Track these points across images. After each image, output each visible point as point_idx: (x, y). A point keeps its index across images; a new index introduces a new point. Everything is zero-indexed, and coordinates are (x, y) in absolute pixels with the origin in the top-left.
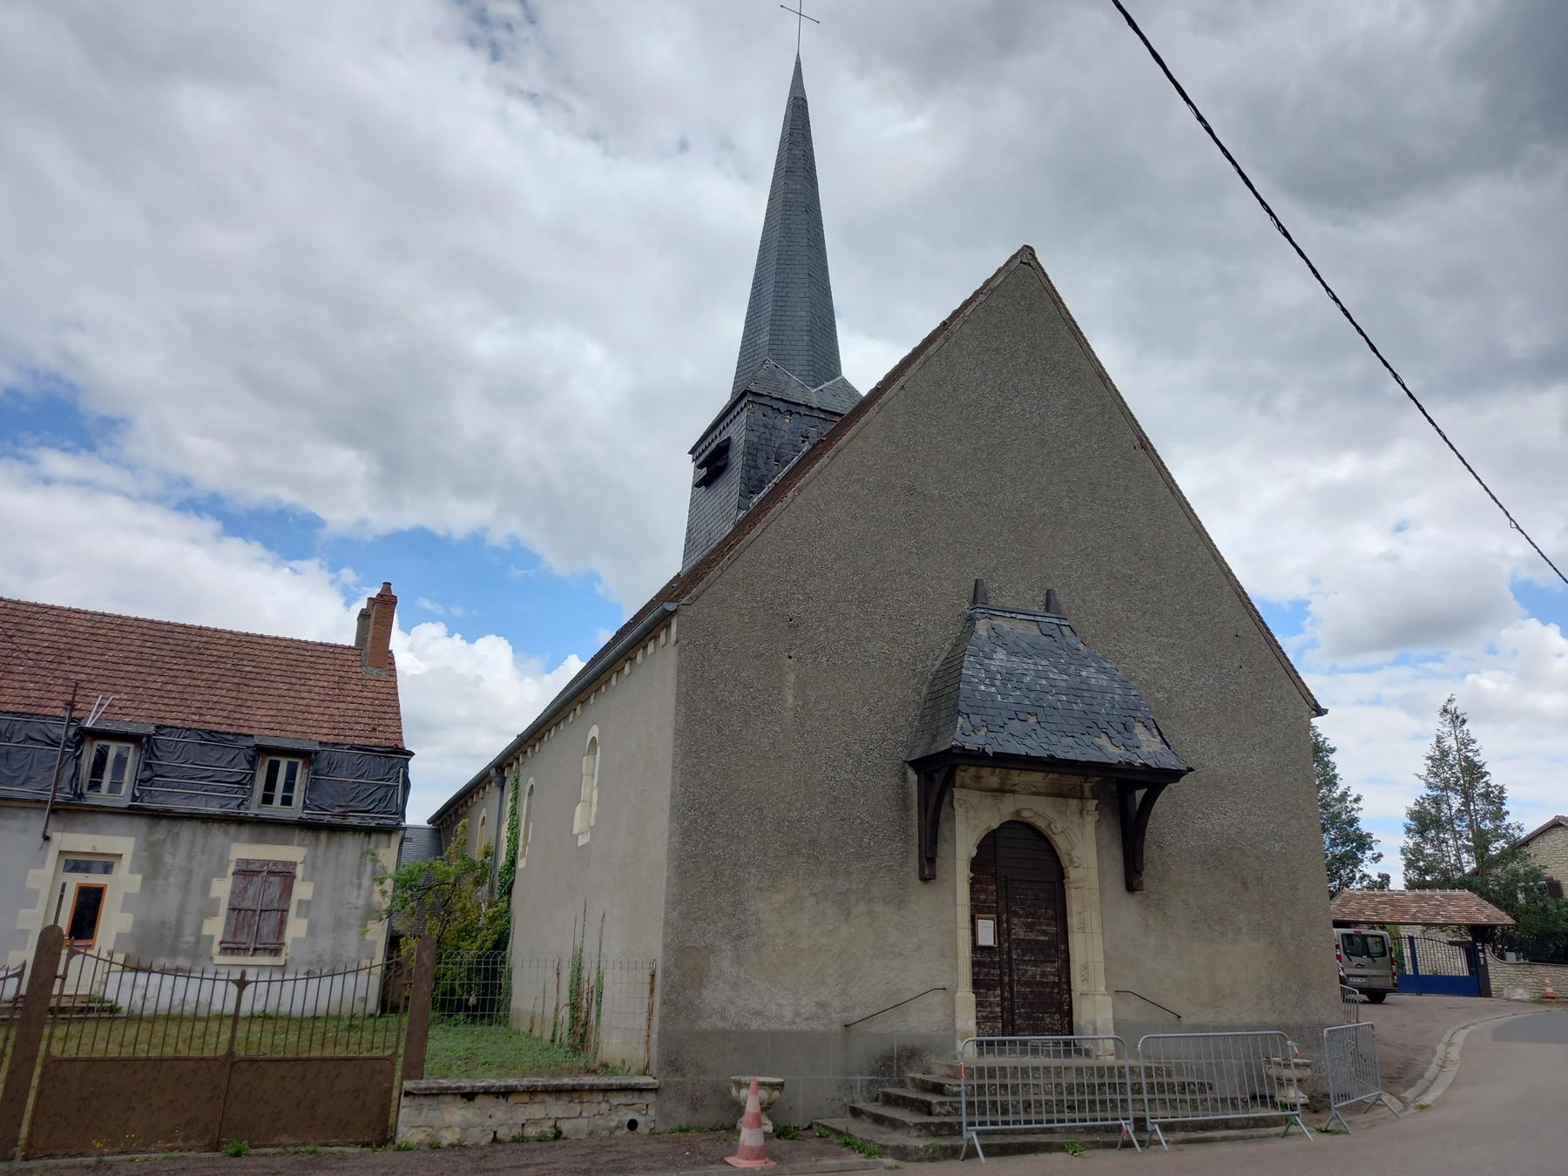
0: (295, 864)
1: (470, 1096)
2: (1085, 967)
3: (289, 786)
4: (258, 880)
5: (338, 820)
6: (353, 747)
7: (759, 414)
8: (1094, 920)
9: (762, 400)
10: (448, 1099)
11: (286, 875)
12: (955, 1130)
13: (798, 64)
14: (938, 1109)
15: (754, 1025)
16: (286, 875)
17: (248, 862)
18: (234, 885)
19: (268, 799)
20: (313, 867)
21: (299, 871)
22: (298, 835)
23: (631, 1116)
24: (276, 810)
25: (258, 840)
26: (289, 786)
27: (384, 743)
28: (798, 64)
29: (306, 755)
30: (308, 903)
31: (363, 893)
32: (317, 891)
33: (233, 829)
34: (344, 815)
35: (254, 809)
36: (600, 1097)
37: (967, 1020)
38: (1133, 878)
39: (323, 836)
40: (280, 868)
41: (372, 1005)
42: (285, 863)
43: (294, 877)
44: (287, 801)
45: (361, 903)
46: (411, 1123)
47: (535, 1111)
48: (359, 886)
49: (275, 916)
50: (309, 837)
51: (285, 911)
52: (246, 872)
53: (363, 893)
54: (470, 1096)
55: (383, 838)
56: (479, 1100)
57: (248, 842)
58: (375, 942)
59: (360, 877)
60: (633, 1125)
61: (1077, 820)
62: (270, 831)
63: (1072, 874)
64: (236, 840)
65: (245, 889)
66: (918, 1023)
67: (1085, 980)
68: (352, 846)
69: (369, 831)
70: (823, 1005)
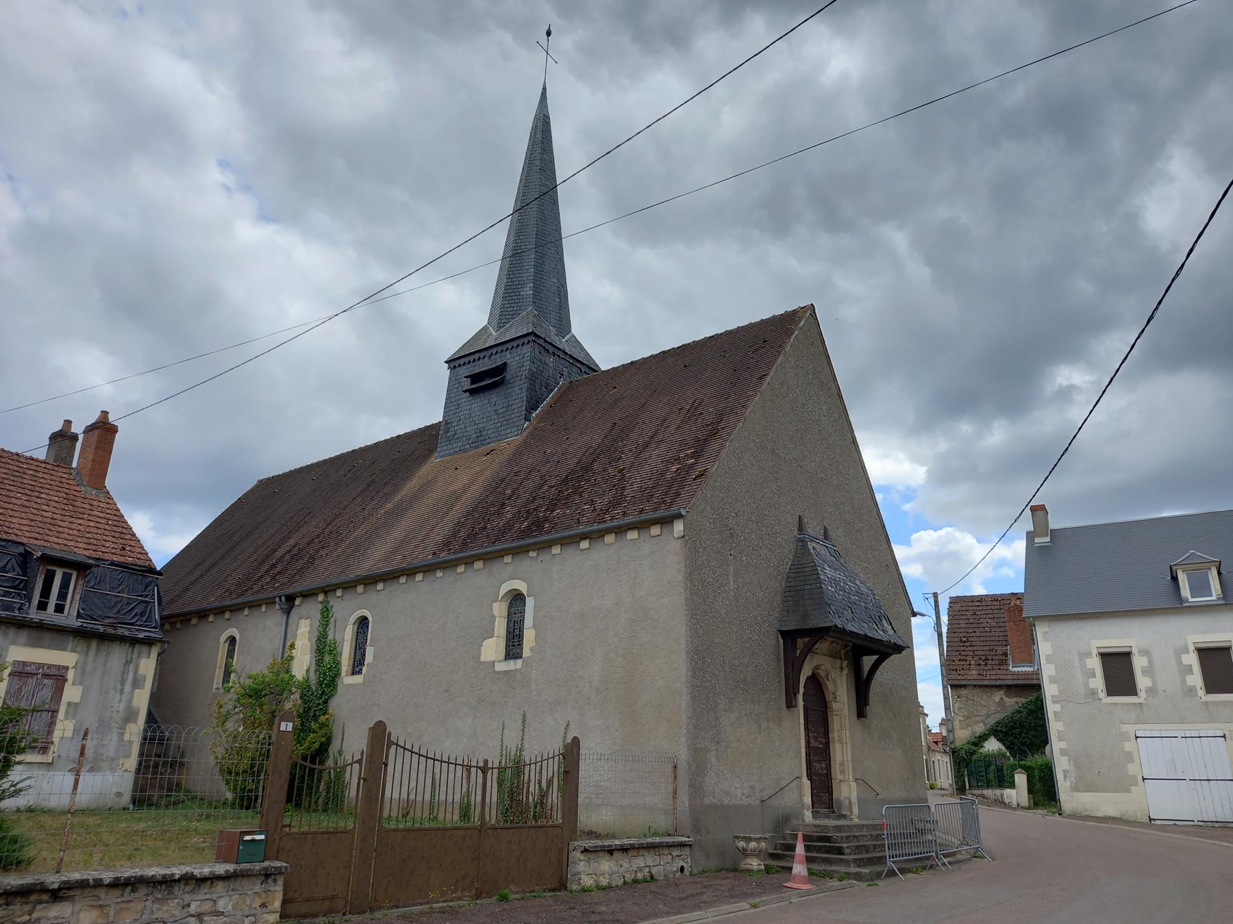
0: (67, 668)
1: (610, 852)
2: (842, 764)
3: (62, 595)
4: (32, 682)
5: (110, 631)
6: (113, 564)
7: (537, 351)
8: (847, 735)
9: (541, 342)
10: (601, 854)
11: (58, 677)
12: (881, 860)
13: (544, 89)
14: (847, 851)
15: (727, 801)
16: (58, 677)
17: (24, 663)
18: (10, 686)
19: (42, 606)
20: (83, 672)
21: (70, 675)
22: (71, 642)
23: (682, 863)
24: (50, 615)
25: (34, 644)
26: (62, 595)
27: (139, 562)
28: (544, 89)
29: (82, 568)
30: (76, 704)
31: (125, 697)
32: (84, 695)
33: (12, 632)
34: (112, 625)
35: (34, 615)
36: (667, 852)
37: (808, 799)
38: (861, 713)
39: (94, 644)
40: (53, 671)
41: (126, 799)
42: (58, 667)
43: (66, 680)
44: (59, 609)
45: (122, 707)
46: (589, 872)
47: (639, 862)
48: (122, 691)
49: (46, 717)
50: (81, 645)
51: (55, 712)
52: (22, 672)
53: (125, 697)
54: (610, 852)
55: (145, 649)
56: (617, 855)
57: (26, 645)
58: (131, 742)
59: (123, 684)
60: (682, 869)
61: (838, 671)
62: (47, 636)
63: (835, 706)
64: (14, 643)
65: (20, 690)
66: (787, 800)
67: (842, 772)
68: (118, 654)
69: (134, 642)
70: (752, 788)
